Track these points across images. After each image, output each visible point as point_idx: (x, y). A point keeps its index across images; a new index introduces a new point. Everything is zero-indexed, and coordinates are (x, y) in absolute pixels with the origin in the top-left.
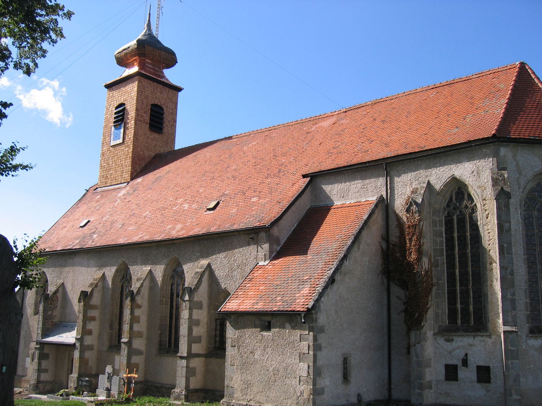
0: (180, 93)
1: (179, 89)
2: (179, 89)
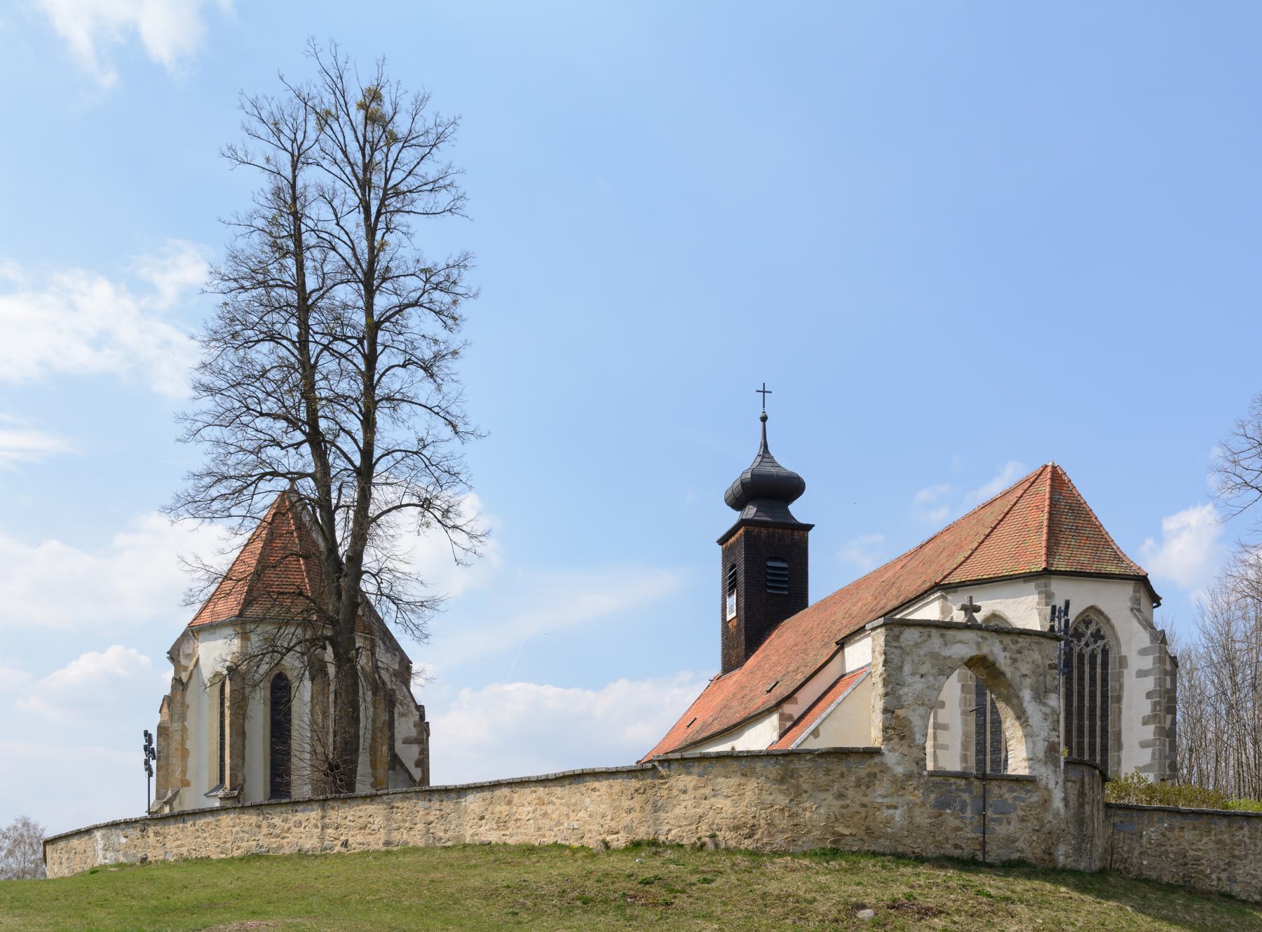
0: (810, 533)
1: (808, 527)
2: (808, 527)
